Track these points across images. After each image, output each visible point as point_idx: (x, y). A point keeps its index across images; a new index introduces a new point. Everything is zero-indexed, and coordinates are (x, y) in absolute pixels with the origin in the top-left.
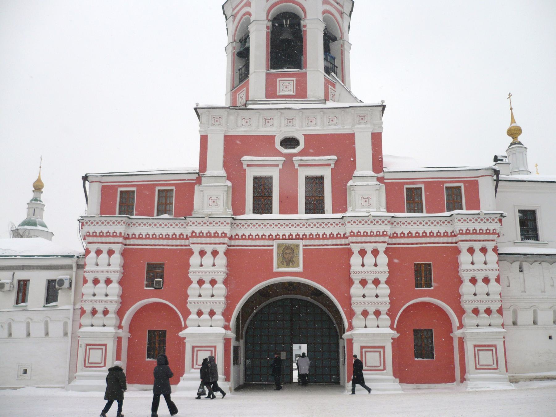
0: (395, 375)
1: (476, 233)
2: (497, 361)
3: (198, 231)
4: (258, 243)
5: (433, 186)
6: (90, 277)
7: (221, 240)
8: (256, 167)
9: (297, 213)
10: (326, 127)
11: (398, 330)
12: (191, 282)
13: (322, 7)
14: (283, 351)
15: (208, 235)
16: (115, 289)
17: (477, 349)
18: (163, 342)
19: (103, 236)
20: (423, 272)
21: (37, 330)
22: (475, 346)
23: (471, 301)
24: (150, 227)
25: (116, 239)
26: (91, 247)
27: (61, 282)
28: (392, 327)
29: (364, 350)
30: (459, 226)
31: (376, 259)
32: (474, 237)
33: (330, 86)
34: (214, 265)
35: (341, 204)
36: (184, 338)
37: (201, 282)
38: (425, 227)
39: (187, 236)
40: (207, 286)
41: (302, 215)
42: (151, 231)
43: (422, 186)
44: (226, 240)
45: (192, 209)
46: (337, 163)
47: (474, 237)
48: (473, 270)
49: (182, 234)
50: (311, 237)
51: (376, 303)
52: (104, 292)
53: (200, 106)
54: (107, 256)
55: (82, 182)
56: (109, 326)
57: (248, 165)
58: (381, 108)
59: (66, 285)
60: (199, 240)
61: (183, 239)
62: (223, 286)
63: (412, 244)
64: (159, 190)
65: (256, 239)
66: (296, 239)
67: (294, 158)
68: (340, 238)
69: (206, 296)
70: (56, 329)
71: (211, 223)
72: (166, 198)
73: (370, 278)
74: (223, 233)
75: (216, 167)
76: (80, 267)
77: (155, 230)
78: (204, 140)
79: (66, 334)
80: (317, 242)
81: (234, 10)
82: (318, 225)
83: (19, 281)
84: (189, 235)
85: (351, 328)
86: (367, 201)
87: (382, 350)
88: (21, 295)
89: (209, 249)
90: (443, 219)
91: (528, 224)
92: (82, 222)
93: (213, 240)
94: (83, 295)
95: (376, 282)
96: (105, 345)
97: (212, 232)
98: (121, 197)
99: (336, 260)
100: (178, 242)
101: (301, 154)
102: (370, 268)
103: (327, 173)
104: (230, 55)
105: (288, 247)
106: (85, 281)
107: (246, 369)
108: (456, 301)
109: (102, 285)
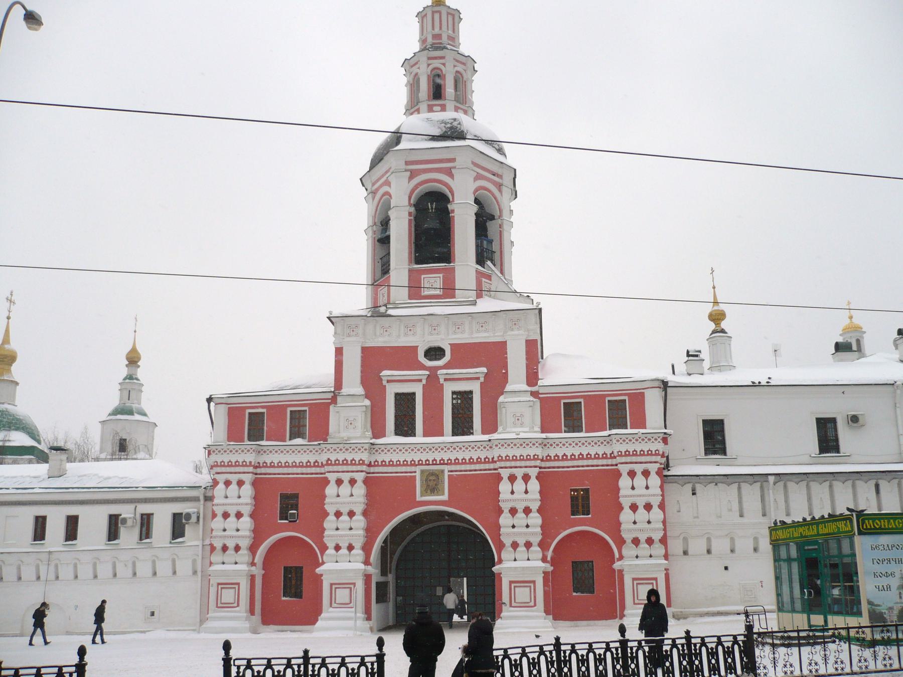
0: (547, 612)
1: (636, 455)
2: (535, 597)
3: (333, 459)
4: (399, 469)
5: (595, 400)
6: (219, 511)
7: (359, 468)
8: (397, 382)
9: (443, 435)
10: (475, 335)
11: (553, 562)
12: (328, 514)
13: (472, 186)
14: (439, 585)
15: (345, 463)
16: (246, 523)
17: (635, 582)
18: (300, 579)
19: (231, 466)
20: (580, 498)
21: (164, 568)
22: (634, 579)
23: (630, 530)
24: (282, 455)
25: (246, 469)
26: (218, 477)
27: (188, 516)
28: (544, 560)
29: (513, 585)
30: (618, 447)
32: (634, 459)
33: (484, 280)
34: (352, 495)
35: (490, 426)
36: (322, 575)
37: (338, 514)
40: (345, 518)
41: (448, 438)
42: (283, 458)
44: (364, 468)
45: (327, 433)
46: (486, 375)
47: (634, 459)
48: (633, 496)
49: (316, 461)
50: (457, 462)
51: (525, 534)
52: (234, 526)
53: (335, 314)
54: (236, 487)
56: (242, 563)
57: (388, 381)
58: (537, 311)
59: (194, 519)
60: (335, 468)
61: (318, 466)
62: (362, 518)
63: (568, 467)
64: (291, 411)
65: (397, 465)
66: (440, 464)
67: (439, 372)
68: (489, 462)
69: (343, 529)
70: (184, 567)
71: (347, 450)
72: (299, 419)
73: (520, 507)
75: (353, 385)
76: (209, 499)
77: (288, 456)
78: (339, 351)
79: (195, 572)
80: (285, 470)
81: (373, 184)
82: (464, 449)
83: (142, 515)
84: (324, 463)
85: (500, 561)
87: (532, 585)
88: (144, 529)
89: (346, 477)
90: (602, 440)
91: (714, 436)
92: (209, 450)
94: (212, 530)
95: (527, 511)
96: (238, 584)
97: (349, 459)
98: (250, 421)
99: (484, 486)
100: (313, 470)
101: (446, 367)
102: (520, 495)
103: (475, 388)
104: (370, 241)
105: (432, 473)
106: (214, 515)
107: (397, 607)
108: (615, 529)
109: (232, 519)
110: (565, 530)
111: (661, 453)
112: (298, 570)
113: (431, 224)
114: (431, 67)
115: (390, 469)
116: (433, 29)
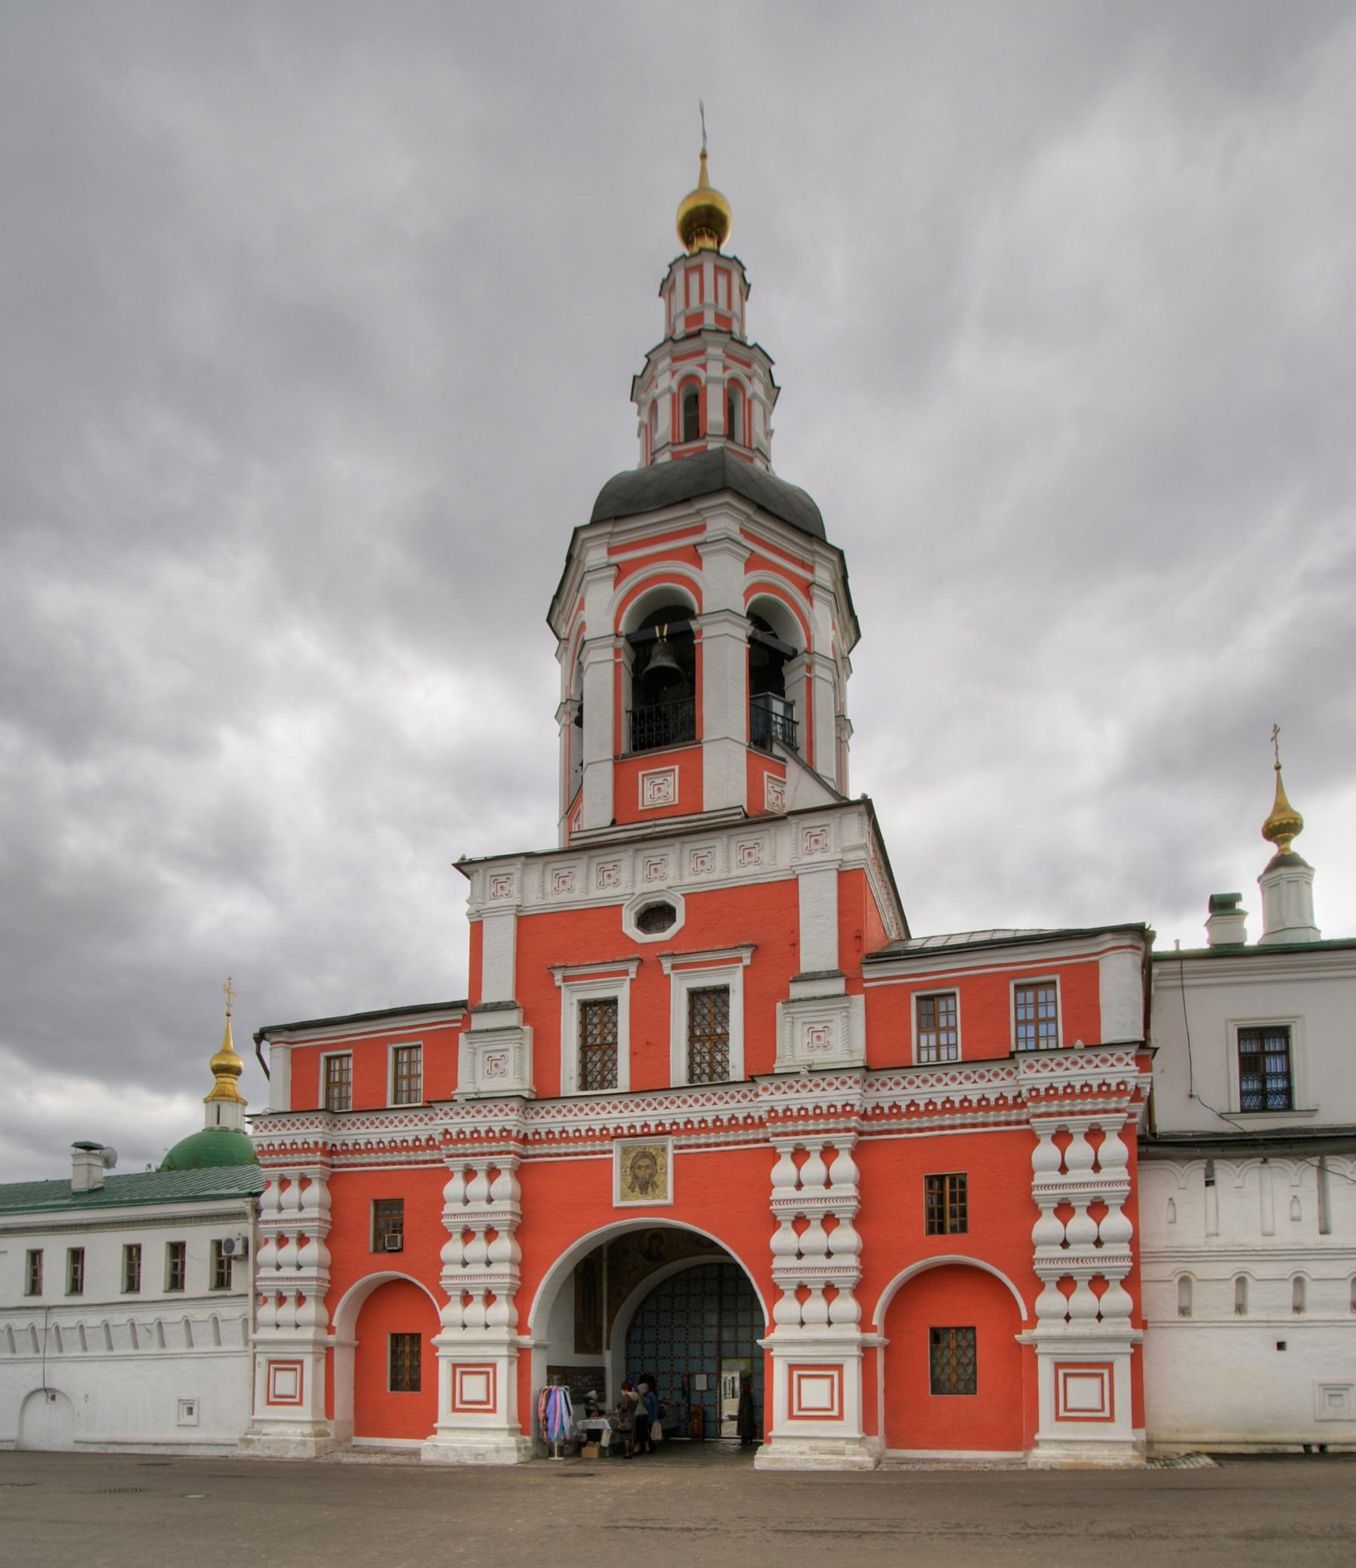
6: (269, 1231)
10: (735, 872)
14: (702, 1372)
15: (476, 1137)
27: (230, 1244)
31: (828, 1168)
32: (1067, 1105)
38: (944, 1089)
39: (760, 1118)
43: (1057, 978)
47: (801, 1126)
48: (1063, 1185)
50: (689, 1128)
55: (254, 1045)
59: (238, 1250)
60: (460, 1148)
74: (505, 1130)
80: (381, 1158)
86: (823, 1036)
87: (835, 1374)
89: (480, 1164)
93: (486, 1147)
110: (901, 1268)
111: (1131, 1087)
112: (415, 1338)
113: (661, 660)
114: (678, 377)
115: (563, 1148)
116: (687, 304)
